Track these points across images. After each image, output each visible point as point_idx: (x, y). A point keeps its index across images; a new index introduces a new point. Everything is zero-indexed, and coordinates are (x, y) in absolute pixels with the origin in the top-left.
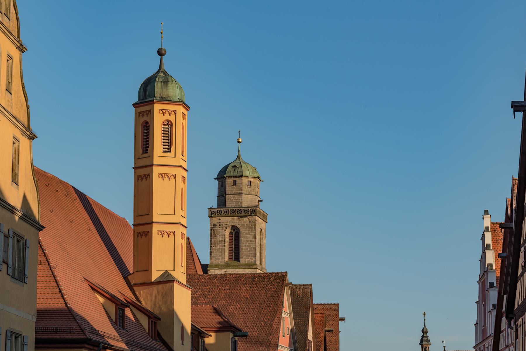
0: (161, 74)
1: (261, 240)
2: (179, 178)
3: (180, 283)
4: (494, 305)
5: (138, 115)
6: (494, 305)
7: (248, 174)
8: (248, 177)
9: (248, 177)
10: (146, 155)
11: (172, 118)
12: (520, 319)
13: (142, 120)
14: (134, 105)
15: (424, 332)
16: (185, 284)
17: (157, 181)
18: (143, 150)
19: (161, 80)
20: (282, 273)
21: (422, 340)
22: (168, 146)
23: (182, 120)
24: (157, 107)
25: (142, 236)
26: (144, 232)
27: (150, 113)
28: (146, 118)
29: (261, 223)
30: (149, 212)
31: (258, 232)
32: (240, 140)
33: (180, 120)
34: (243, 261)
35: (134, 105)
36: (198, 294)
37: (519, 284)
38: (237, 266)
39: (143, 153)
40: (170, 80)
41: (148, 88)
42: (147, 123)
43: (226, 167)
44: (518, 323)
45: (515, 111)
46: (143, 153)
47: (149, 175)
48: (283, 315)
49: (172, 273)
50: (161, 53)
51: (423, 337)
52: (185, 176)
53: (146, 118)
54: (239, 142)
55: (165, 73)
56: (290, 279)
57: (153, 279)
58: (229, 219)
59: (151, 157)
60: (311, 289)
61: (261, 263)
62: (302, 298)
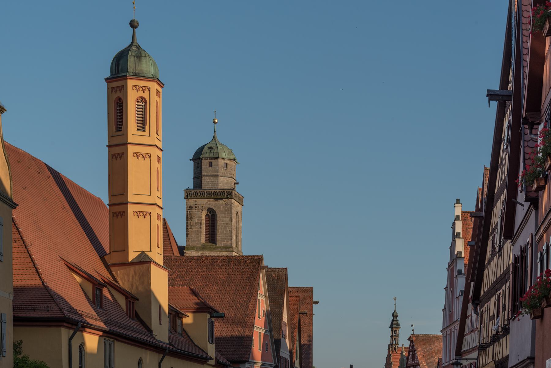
0: (134, 48)
1: (237, 223)
2: (154, 158)
3: (156, 264)
4: (461, 291)
5: (111, 90)
6: (461, 291)
7: (224, 156)
8: (224, 159)
9: (224, 159)
10: (120, 133)
11: (146, 95)
12: (486, 306)
13: (115, 96)
14: (107, 80)
15: (395, 316)
16: (162, 265)
17: (131, 161)
18: (117, 128)
19: (134, 54)
20: (257, 256)
21: (392, 324)
22: (143, 124)
23: (156, 98)
24: (130, 83)
25: (117, 216)
26: (120, 212)
27: (123, 88)
28: (119, 94)
29: (237, 206)
30: (124, 191)
31: (234, 215)
32: (216, 121)
33: (154, 98)
34: (219, 244)
35: (107, 80)
36: (175, 276)
37: (486, 272)
38: (214, 248)
39: (117, 131)
40: (143, 55)
41: (121, 62)
42: (120, 99)
43: (202, 148)
44: (484, 308)
45: (490, 100)
46: (117, 131)
47: (123, 154)
48: (259, 298)
49: (149, 254)
50: (133, 25)
51: (393, 321)
52: (161, 156)
53: (119, 94)
54: (215, 123)
55: (138, 47)
56: (266, 262)
57: (130, 259)
58: (205, 201)
59: (125, 135)
60: (286, 273)
61: (237, 247)
62: (278, 281)
